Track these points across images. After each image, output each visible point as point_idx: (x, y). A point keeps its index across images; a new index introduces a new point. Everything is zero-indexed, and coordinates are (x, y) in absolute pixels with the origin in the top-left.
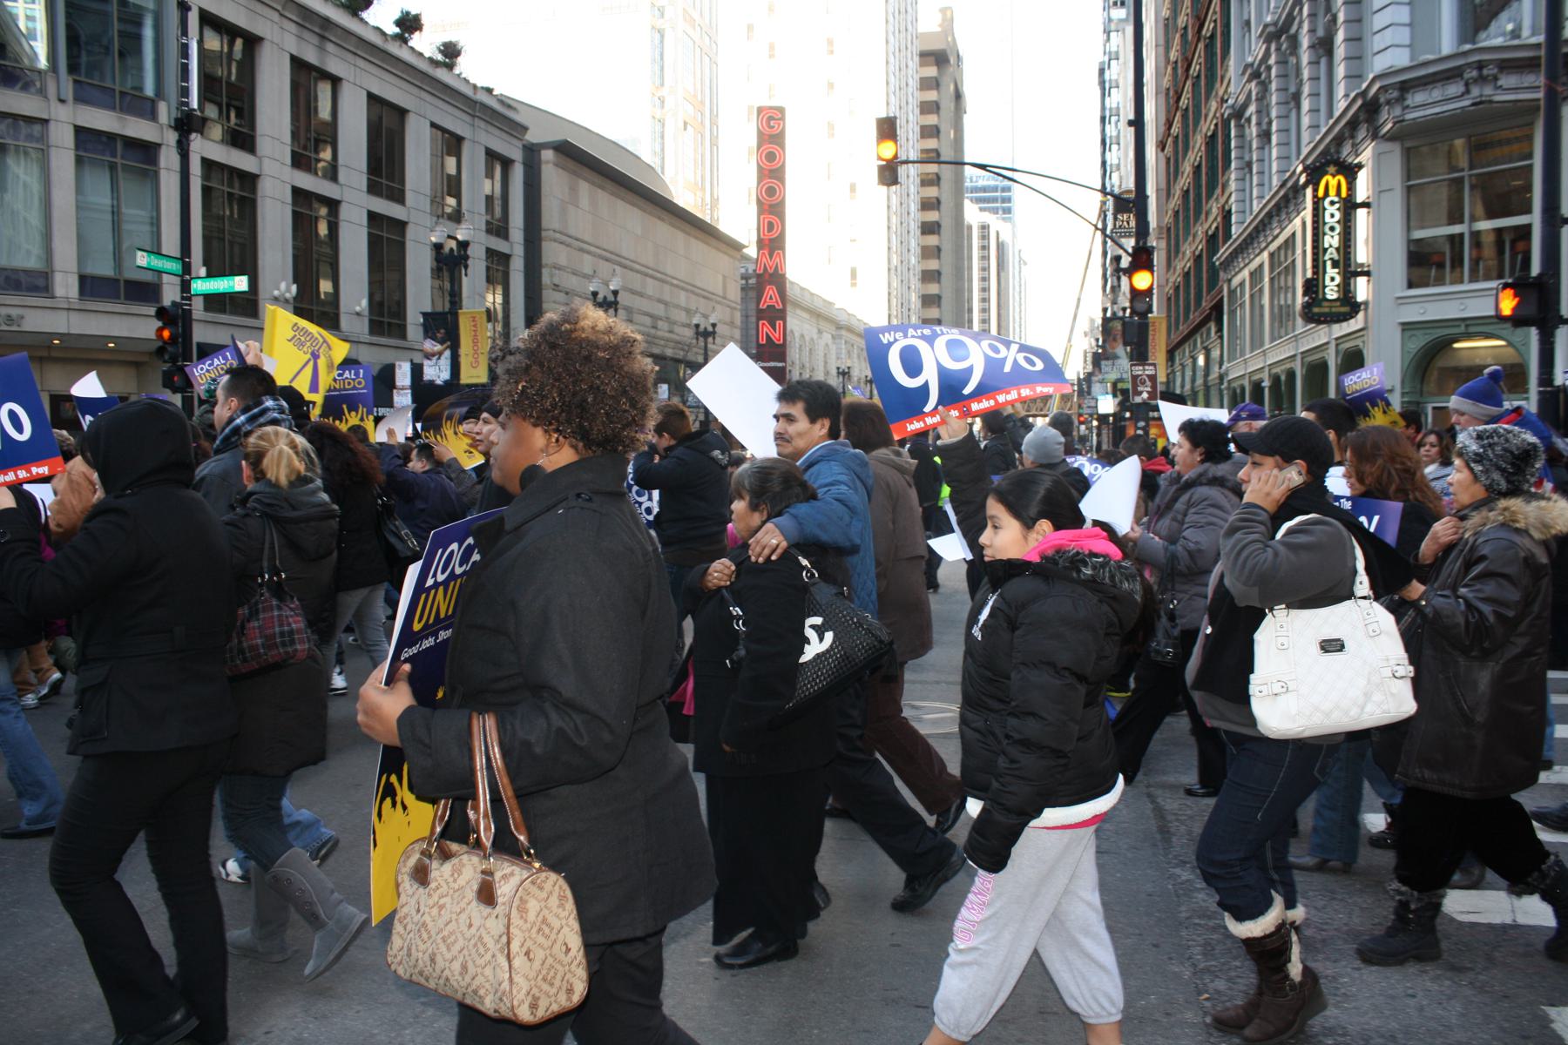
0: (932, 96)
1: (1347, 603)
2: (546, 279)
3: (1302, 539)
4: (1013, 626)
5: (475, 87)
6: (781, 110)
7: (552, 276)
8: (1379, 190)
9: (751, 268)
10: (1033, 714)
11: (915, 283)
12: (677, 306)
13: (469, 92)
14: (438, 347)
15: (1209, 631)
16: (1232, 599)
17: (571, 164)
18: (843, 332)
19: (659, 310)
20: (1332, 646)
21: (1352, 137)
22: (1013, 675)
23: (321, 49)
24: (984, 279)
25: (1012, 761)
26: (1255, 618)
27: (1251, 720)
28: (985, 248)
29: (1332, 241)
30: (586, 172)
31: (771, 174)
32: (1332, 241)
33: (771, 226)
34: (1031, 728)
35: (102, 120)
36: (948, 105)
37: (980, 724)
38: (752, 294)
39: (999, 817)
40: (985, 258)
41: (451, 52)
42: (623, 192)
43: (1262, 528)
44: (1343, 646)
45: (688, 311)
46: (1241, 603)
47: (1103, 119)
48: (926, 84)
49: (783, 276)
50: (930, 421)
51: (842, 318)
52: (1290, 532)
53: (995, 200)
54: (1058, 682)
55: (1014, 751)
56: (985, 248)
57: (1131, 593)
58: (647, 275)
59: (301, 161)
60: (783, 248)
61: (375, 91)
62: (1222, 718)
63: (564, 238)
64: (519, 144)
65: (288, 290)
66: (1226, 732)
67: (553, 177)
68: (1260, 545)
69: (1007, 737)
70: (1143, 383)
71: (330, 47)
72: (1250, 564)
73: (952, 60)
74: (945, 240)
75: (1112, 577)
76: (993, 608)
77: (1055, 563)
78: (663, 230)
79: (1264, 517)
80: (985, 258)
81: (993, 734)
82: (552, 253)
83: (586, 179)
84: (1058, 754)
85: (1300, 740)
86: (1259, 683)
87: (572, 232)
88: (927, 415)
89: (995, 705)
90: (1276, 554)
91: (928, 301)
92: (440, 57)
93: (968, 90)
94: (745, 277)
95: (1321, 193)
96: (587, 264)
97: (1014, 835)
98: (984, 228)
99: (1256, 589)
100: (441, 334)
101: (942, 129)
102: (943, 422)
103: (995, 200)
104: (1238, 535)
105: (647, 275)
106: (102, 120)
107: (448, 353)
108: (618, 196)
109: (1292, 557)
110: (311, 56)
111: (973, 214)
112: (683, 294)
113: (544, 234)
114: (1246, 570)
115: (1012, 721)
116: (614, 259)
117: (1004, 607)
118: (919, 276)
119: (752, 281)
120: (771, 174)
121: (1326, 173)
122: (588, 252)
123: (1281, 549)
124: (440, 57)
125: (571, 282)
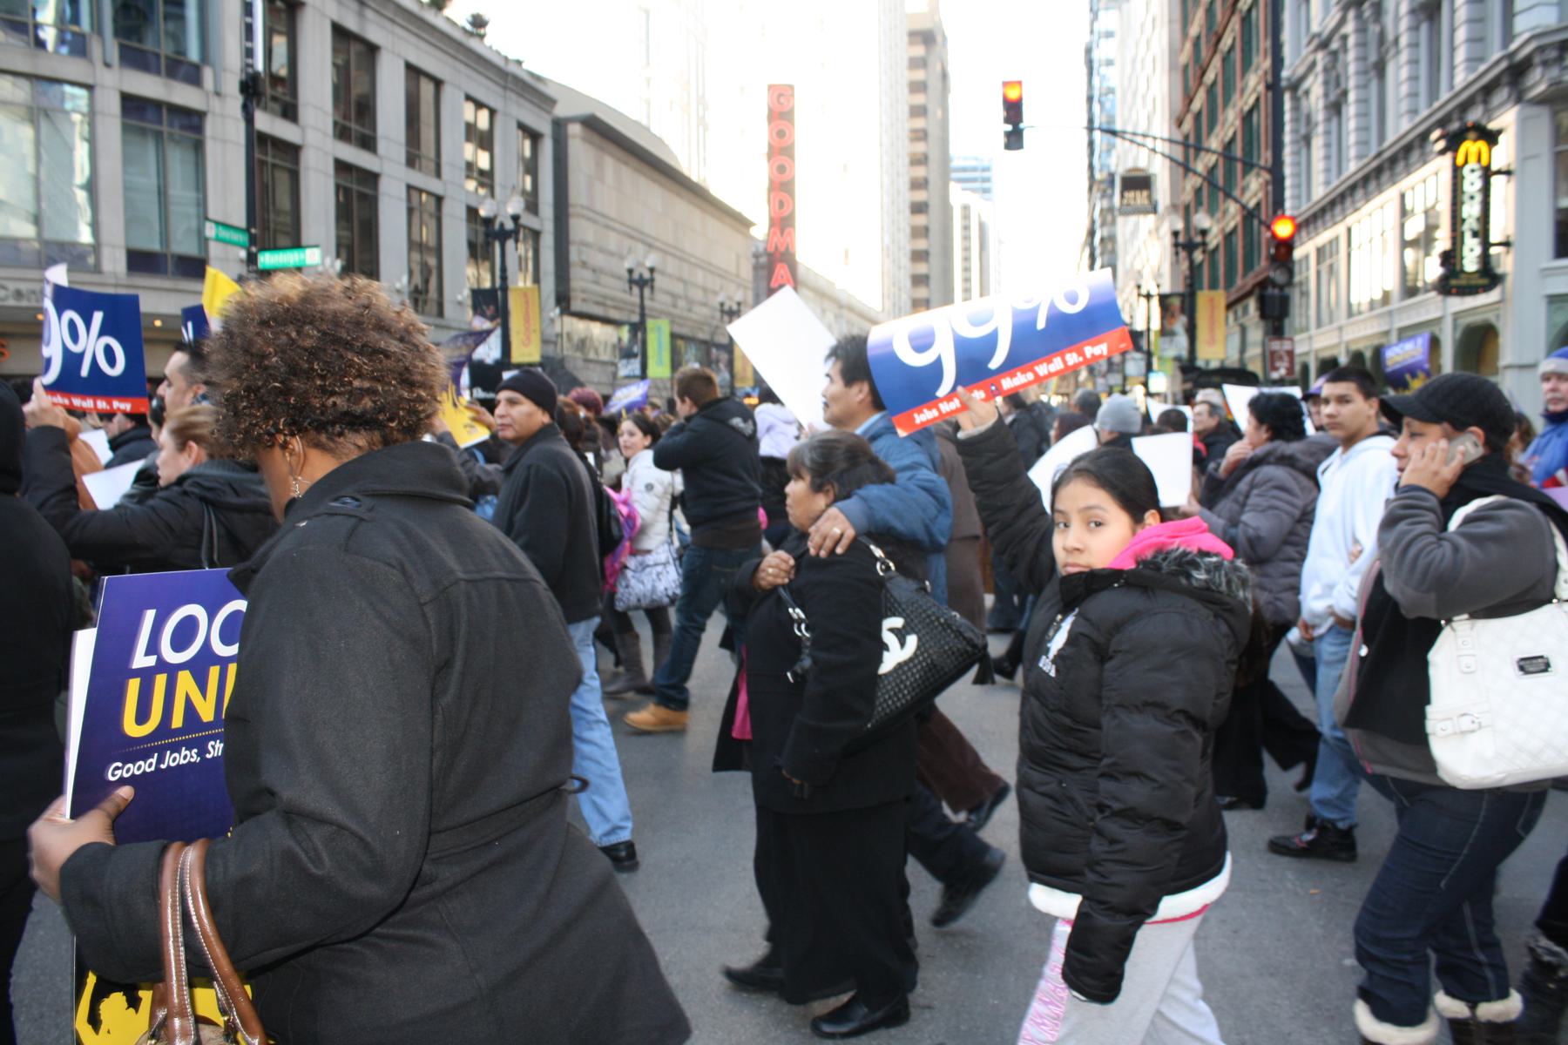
0: (919, 75)
1: (1547, 608)
2: (574, 256)
3: (1487, 528)
4: (1102, 655)
5: (506, 59)
6: (791, 87)
7: (580, 253)
8: (1524, 156)
9: (761, 249)
10: (1137, 775)
11: (905, 261)
12: (695, 285)
13: (501, 63)
14: (487, 325)
15: (1364, 651)
16: (1396, 605)
17: (596, 139)
18: (845, 312)
19: (678, 288)
20: (1533, 665)
21: (1485, 102)
22: (1106, 721)
23: (361, 15)
24: (967, 259)
25: (1113, 841)
26: (1429, 632)
27: (1430, 764)
28: (966, 228)
29: (1471, 210)
30: (611, 148)
31: (781, 151)
32: (1471, 210)
33: (781, 204)
34: (1136, 794)
35: (149, 86)
36: (934, 84)
37: (1052, 787)
38: (764, 273)
39: (1102, 920)
40: (966, 238)
41: (479, 22)
42: (646, 169)
43: (1431, 517)
44: (1548, 665)
45: (705, 290)
46: (1410, 614)
47: (1090, 99)
48: (916, 63)
49: (793, 255)
50: (945, 407)
51: (843, 298)
52: (1468, 520)
53: (974, 180)
54: (1170, 729)
55: (1113, 827)
56: (966, 228)
57: (1243, 604)
58: (666, 253)
59: (372, 178)
60: (793, 226)
61: (414, 60)
62: (1390, 762)
63: (590, 214)
64: (548, 118)
65: (333, 266)
66: (1394, 780)
67: (580, 150)
68: (1432, 539)
69: (1101, 808)
70: (1281, 358)
71: (369, 14)
72: (1422, 563)
73: (939, 39)
74: (930, 219)
75: (1229, 582)
76: (1070, 633)
77: (1158, 568)
78: (682, 208)
79: (1433, 502)
80: (966, 238)
81: (1072, 800)
82: (580, 229)
83: (613, 156)
84: (1172, 826)
85: (1498, 789)
86: (1437, 718)
87: (598, 207)
88: (941, 400)
89: (1075, 761)
90: (1456, 549)
91: (919, 280)
92: (469, 27)
93: (951, 70)
94: (756, 256)
95: (1460, 161)
96: (613, 241)
97: (1125, 945)
98: (966, 208)
99: (1433, 596)
100: (490, 311)
101: (930, 108)
102: (964, 407)
103: (974, 180)
104: (1402, 526)
105: (666, 253)
106: (149, 86)
107: (498, 332)
108: (639, 172)
109: (1477, 552)
110: (351, 23)
111: (958, 196)
112: (612, 247)
113: (571, 210)
114: (1419, 569)
115: (1106, 785)
116: (635, 235)
117: (1087, 630)
118: (909, 255)
119: (763, 260)
120: (781, 151)
121: (1464, 139)
122: (614, 229)
123: (1462, 542)
124: (469, 27)
125: (598, 260)
